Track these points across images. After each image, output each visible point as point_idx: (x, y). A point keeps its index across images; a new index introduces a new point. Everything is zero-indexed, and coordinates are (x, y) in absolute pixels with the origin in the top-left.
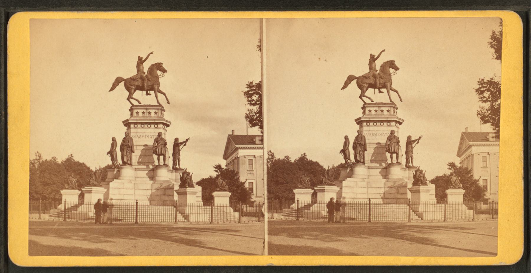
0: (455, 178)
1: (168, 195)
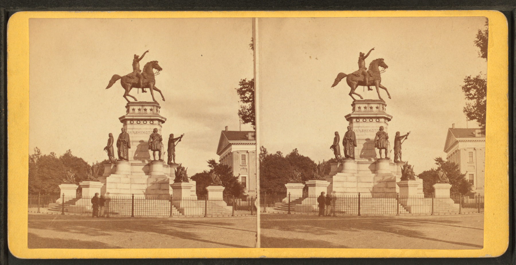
0: (442, 173)
1: (163, 190)
